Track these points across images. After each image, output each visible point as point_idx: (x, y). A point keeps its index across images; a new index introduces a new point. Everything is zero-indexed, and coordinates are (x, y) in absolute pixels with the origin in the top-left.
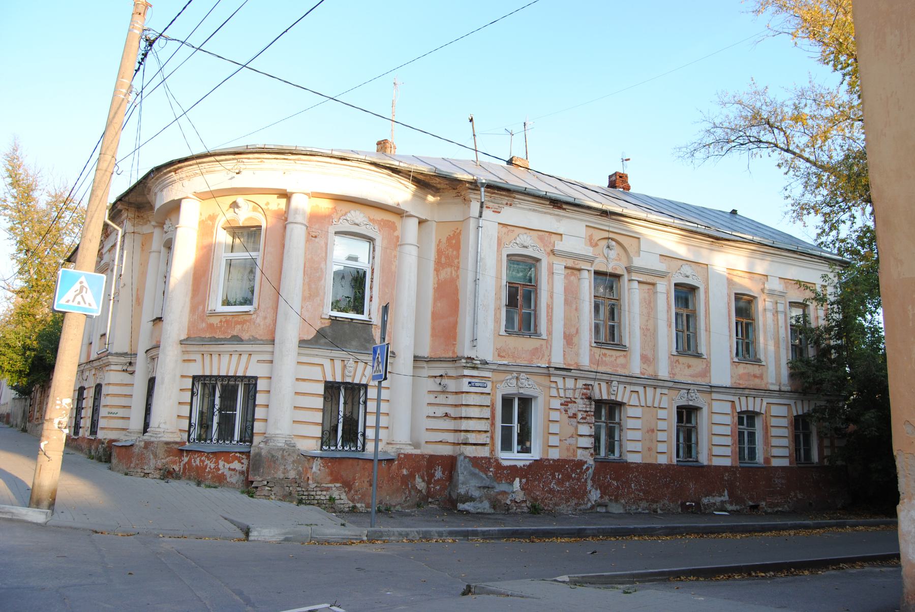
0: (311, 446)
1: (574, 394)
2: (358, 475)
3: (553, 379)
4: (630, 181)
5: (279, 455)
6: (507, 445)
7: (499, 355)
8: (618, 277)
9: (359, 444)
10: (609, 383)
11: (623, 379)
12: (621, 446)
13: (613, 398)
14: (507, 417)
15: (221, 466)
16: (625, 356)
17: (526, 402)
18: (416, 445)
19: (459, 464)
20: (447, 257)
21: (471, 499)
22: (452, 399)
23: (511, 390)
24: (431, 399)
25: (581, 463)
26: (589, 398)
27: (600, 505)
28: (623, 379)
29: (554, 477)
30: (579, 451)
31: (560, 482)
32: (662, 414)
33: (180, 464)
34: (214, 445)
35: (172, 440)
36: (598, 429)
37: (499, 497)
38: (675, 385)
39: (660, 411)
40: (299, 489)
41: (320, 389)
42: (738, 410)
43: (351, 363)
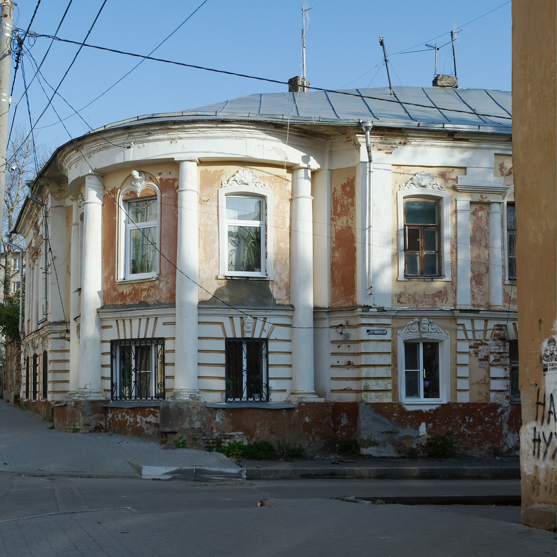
0: (216, 399)
1: (485, 334)
2: (258, 424)
3: (459, 322)
5: (185, 407)
6: (412, 391)
7: (398, 301)
14: (411, 361)
15: (138, 420)
17: (432, 348)
19: (361, 410)
20: (343, 205)
21: (374, 444)
23: (413, 336)
25: (495, 406)
26: (503, 339)
29: (464, 421)
30: (492, 395)
31: (471, 427)
33: (103, 416)
34: (134, 402)
35: (98, 399)
37: (403, 442)
40: (204, 437)
41: (221, 345)
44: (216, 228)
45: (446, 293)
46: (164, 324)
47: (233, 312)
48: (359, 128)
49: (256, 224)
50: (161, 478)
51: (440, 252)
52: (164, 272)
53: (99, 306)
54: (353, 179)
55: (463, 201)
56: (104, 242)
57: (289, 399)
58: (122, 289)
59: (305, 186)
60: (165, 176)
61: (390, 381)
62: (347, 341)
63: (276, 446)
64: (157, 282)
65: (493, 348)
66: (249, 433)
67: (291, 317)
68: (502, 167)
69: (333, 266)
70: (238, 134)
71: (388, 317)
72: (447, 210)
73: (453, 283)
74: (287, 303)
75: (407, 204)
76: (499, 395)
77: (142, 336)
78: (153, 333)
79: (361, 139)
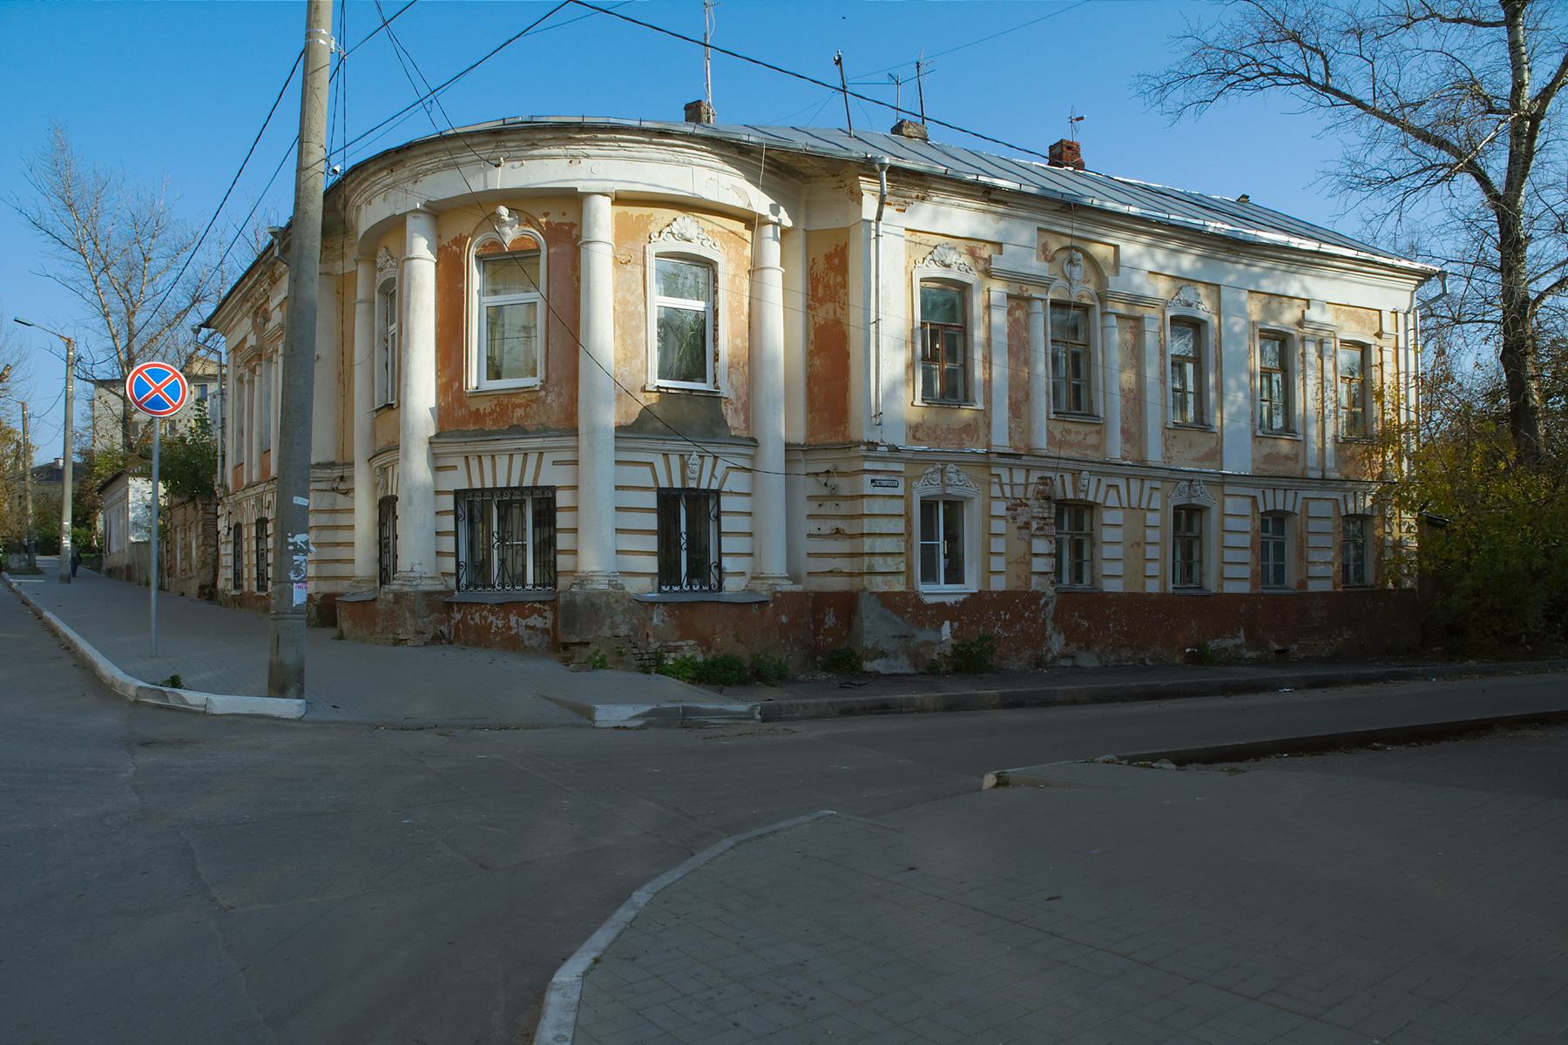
0: (643, 587)
4: (1084, 156)
6: (929, 575)
8: (1086, 309)
9: (713, 581)
10: (1076, 474)
11: (1096, 468)
12: (1092, 568)
13: (1082, 496)
14: (928, 531)
15: (513, 623)
16: (1099, 432)
17: (954, 507)
18: (794, 578)
20: (827, 286)
21: (883, 654)
22: (845, 508)
23: (933, 491)
24: (813, 508)
25: (1037, 596)
26: (1048, 499)
27: (1064, 656)
28: (1096, 468)
30: (1034, 579)
31: (1007, 625)
32: (1153, 519)
33: (450, 618)
34: (495, 594)
36: (1059, 543)
38: (1170, 475)
39: (1149, 515)
41: (651, 500)
42: (1262, 510)
43: (694, 459)
44: (641, 308)
45: (977, 427)
46: (555, 463)
47: (669, 446)
48: (869, 167)
49: (699, 305)
50: (628, 724)
51: (966, 368)
52: (553, 376)
53: (432, 433)
54: (846, 246)
55: (998, 289)
56: (440, 325)
57: (752, 586)
58: (474, 405)
59: (773, 250)
60: (555, 219)
61: (903, 558)
62: (834, 496)
63: (747, 664)
64: (542, 393)
65: (1036, 511)
66: (705, 642)
67: (752, 457)
68: (1045, 248)
69: (811, 379)
70: (681, 158)
71: (900, 460)
72: (978, 302)
73: (986, 414)
74: (745, 434)
75: (923, 292)
76: (1042, 579)
77: (514, 483)
78: (536, 479)
79: (867, 186)
